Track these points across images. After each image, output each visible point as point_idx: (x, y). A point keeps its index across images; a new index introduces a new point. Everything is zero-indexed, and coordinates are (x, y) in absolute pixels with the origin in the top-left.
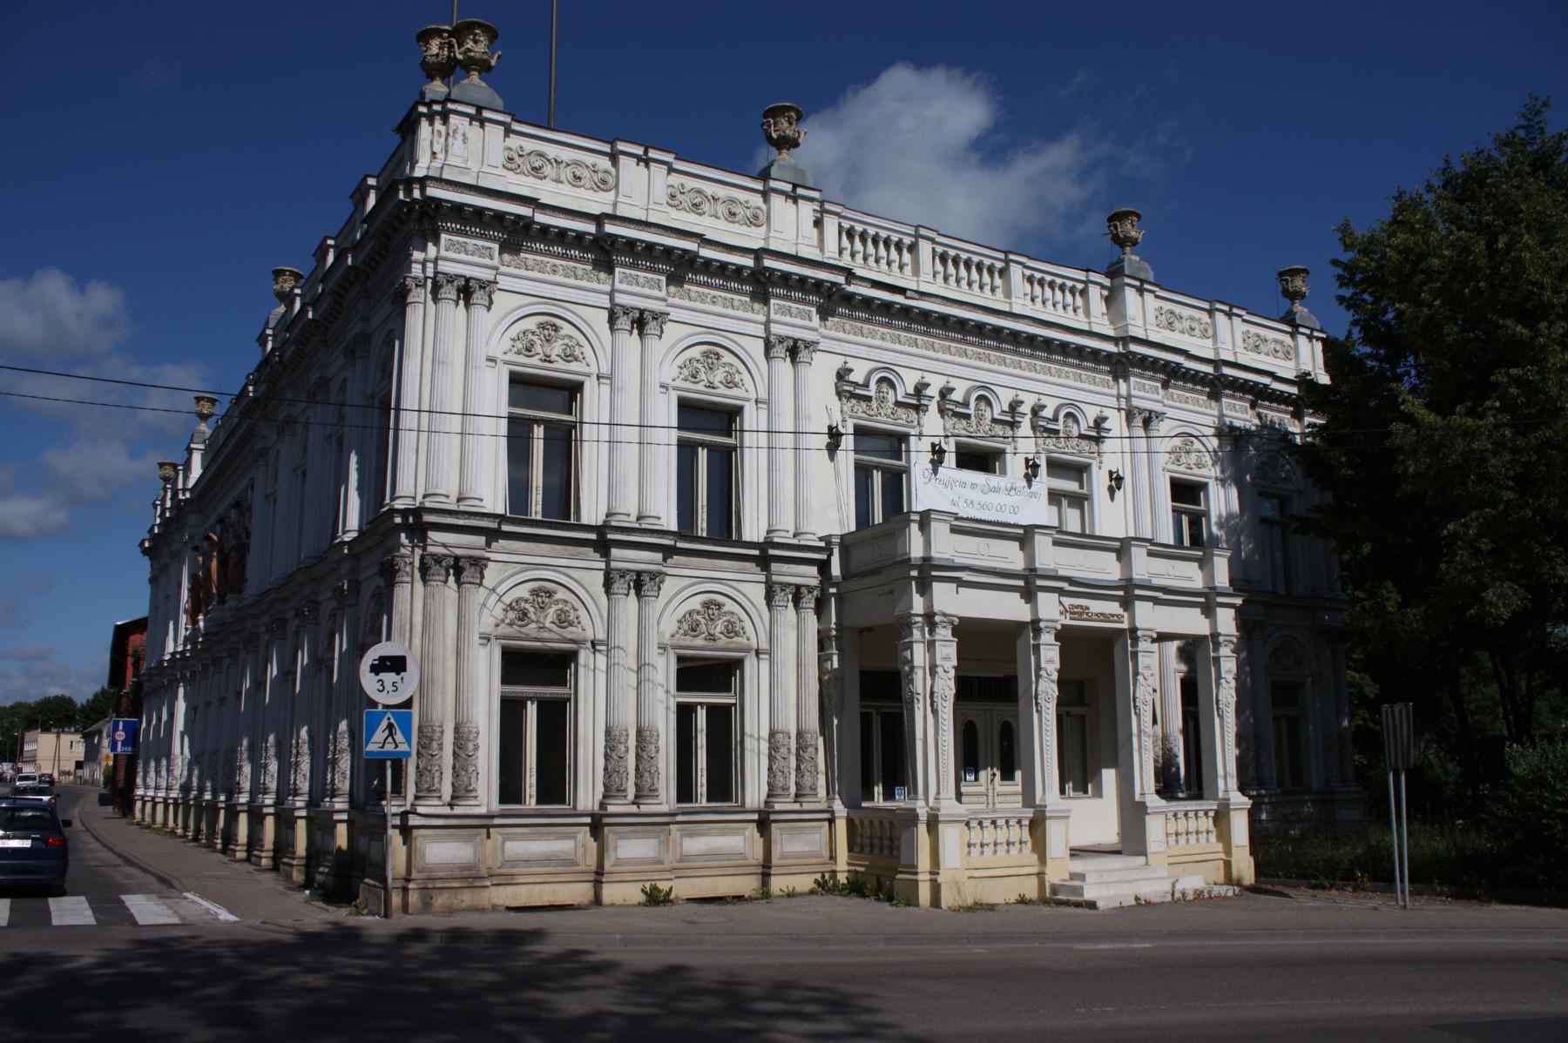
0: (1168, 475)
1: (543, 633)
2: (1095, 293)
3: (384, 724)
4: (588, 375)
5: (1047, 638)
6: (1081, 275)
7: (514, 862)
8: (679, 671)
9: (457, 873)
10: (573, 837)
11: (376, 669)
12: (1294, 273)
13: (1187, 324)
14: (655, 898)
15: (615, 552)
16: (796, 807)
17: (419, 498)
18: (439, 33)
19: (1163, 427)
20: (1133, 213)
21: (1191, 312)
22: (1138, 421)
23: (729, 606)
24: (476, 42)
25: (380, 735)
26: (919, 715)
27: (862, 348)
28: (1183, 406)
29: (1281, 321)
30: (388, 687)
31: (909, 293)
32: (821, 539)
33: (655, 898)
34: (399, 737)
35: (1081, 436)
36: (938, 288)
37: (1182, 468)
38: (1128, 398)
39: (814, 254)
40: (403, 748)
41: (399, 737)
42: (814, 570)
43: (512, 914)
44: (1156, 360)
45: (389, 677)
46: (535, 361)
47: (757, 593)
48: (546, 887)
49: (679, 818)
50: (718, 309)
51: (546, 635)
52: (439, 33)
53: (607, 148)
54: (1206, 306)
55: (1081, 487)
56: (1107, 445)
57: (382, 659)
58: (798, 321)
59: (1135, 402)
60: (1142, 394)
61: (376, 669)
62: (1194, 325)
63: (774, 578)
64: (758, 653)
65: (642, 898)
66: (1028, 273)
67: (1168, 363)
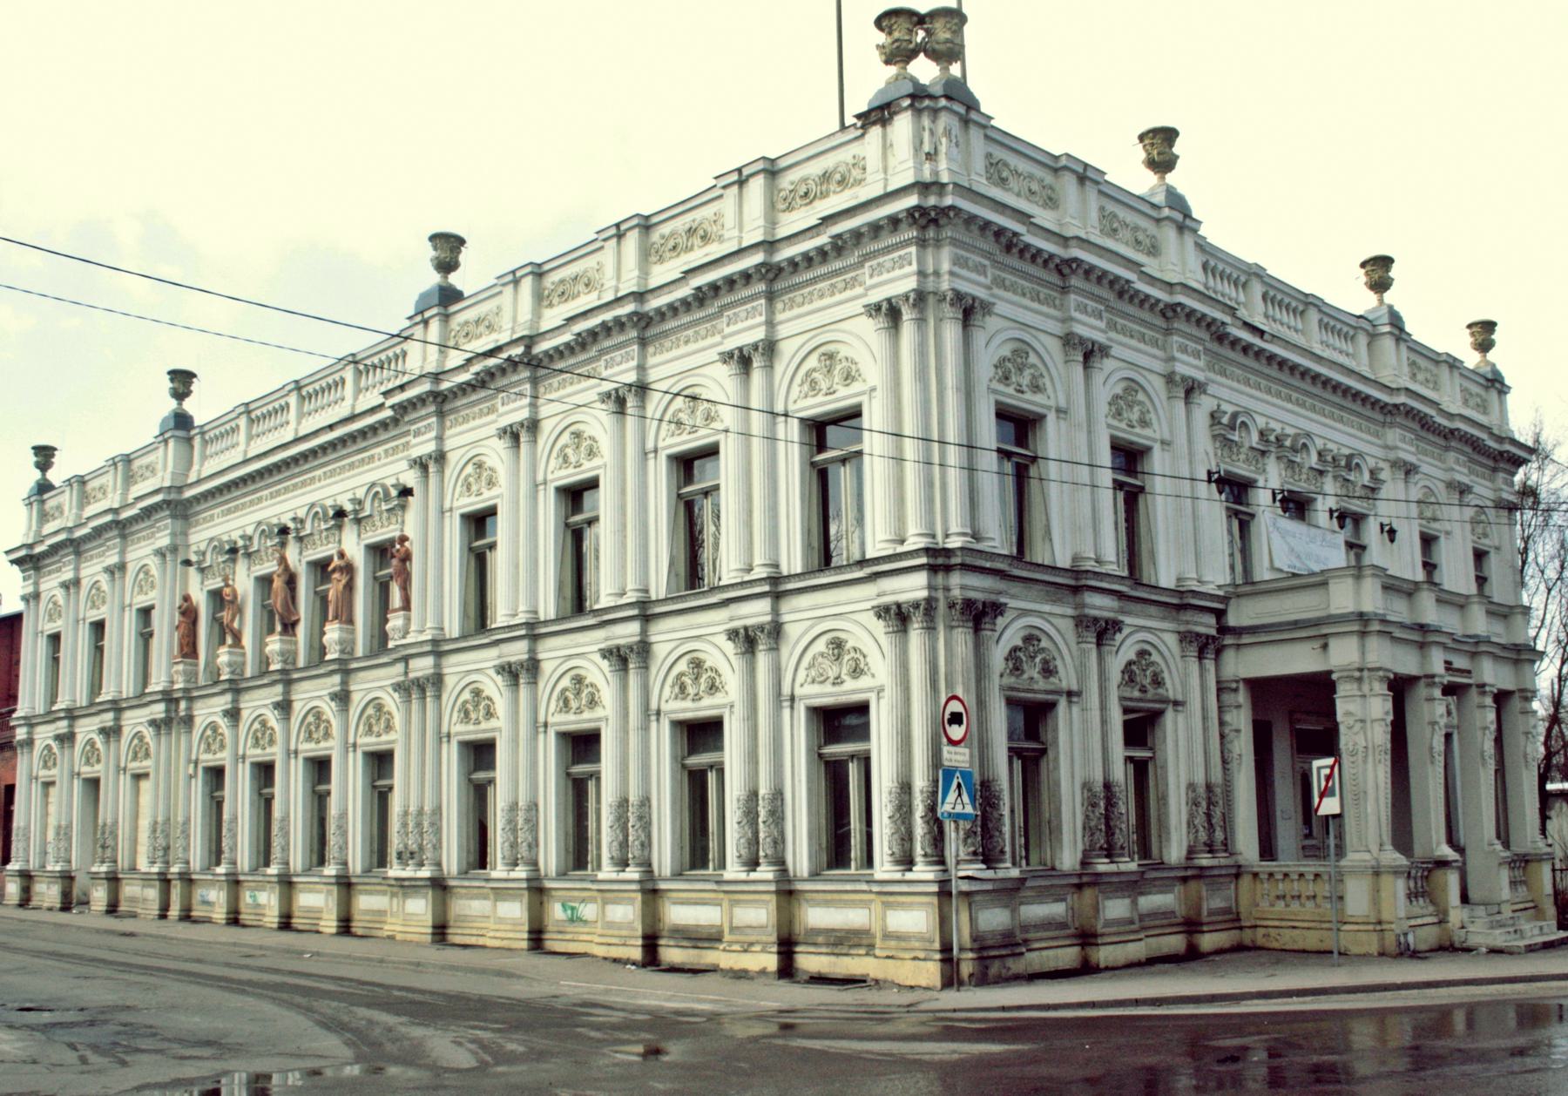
0: (992, 398)
4: (1049, 408)
7: (1025, 928)
8: (1126, 724)
23: (1155, 657)
27: (1229, 392)
31: (1266, 337)
36: (1318, 349)
37: (1123, 425)
39: (1365, 370)
42: (1212, 620)
44: (1105, 273)
46: (1010, 390)
48: (1051, 953)
66: (1326, 320)
67: (1117, 278)
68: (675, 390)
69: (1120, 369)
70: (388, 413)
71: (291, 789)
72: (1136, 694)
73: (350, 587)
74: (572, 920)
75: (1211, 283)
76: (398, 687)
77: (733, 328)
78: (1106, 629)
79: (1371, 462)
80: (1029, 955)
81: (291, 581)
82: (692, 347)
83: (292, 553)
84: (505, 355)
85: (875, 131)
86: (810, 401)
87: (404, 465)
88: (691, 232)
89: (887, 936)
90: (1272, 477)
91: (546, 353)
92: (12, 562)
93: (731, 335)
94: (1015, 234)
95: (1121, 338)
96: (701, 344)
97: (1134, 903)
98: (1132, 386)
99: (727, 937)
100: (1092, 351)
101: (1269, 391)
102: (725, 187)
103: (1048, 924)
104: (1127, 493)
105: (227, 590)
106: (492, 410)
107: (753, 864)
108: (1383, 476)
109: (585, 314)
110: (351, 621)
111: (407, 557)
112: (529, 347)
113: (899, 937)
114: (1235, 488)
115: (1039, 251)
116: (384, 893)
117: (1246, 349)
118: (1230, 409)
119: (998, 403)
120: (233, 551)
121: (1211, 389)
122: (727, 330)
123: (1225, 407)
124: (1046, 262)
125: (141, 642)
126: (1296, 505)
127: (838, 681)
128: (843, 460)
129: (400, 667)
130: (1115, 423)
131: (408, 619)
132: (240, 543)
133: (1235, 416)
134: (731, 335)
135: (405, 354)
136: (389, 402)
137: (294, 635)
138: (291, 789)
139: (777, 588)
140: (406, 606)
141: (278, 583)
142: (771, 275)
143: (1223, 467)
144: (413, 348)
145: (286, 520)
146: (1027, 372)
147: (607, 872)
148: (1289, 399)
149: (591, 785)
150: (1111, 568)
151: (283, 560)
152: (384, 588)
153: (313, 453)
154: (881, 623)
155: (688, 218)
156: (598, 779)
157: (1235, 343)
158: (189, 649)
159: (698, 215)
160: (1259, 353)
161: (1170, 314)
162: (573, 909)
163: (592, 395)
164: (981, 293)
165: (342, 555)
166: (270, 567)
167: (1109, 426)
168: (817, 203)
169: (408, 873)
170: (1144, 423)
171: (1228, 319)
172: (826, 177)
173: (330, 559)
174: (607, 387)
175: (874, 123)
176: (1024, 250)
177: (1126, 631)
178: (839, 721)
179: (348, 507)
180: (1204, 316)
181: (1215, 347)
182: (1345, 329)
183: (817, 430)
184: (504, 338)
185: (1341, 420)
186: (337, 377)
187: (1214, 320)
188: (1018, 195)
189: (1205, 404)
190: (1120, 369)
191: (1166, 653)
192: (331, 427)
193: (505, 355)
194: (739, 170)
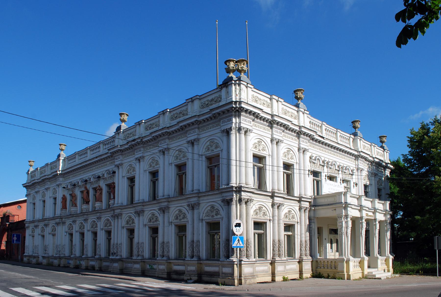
1: (260, 218)
2: (351, 140)
3: (237, 239)
5: (364, 221)
6: (349, 135)
9: (250, 275)
10: (266, 266)
11: (236, 226)
12: (298, 90)
13: (290, 114)
14: (285, 280)
15: (275, 198)
16: (280, 259)
17: (238, 184)
18: (233, 61)
19: (282, 145)
20: (302, 90)
21: (263, 97)
22: (359, 171)
24: (244, 65)
25: (236, 242)
26: (343, 237)
28: (288, 139)
29: (295, 106)
30: (238, 231)
32: (310, 196)
33: (285, 280)
34: (241, 242)
35: (350, 174)
38: (358, 165)
40: (242, 245)
41: (241, 242)
42: (308, 203)
43: (259, 284)
45: (238, 228)
47: (297, 208)
49: (258, 262)
50: (290, 140)
51: (261, 218)
52: (233, 61)
53: (269, 96)
54: (370, 144)
55: (347, 185)
56: (354, 176)
57: (237, 224)
58: (248, 123)
59: (359, 166)
60: (277, 134)
61: (236, 226)
62: (265, 103)
63: (302, 205)
64: (270, 220)
65: (282, 279)
66: (342, 135)
68: (177, 149)
69: (255, 136)
70: (109, 154)
71: (88, 238)
72: (288, 220)
73: (101, 193)
74: (151, 268)
75: (312, 126)
76: (112, 216)
77: (189, 136)
78: (248, 201)
79: (352, 168)
80: (257, 278)
81: (88, 192)
82: (180, 140)
83: (88, 186)
84: (136, 141)
85: (224, 90)
86: (208, 153)
87: (114, 166)
88: (180, 113)
89: (223, 273)
90: (325, 172)
91: (146, 141)
92: (24, 187)
93: (189, 137)
94: (259, 114)
95: (286, 139)
96: (182, 139)
97: (285, 267)
98: (289, 150)
99: (186, 273)
100: (247, 131)
101: (326, 151)
102: (188, 102)
103: (263, 271)
104: (287, 175)
105: (73, 194)
106: (134, 154)
107: (192, 257)
108: (354, 171)
109: (155, 132)
110: (101, 201)
111: (114, 187)
112: (142, 139)
113: (225, 274)
114: (315, 174)
115: (265, 118)
116: (109, 262)
117: (319, 142)
118: (315, 155)
119: (253, 154)
120: (74, 185)
121: (310, 151)
122: (188, 136)
123: (313, 155)
124: (281, 125)
125: (54, 205)
126: (331, 178)
127: (213, 216)
128: (215, 166)
129: (112, 212)
130: (284, 158)
131: (114, 201)
132: (76, 183)
133: (316, 157)
134: (189, 137)
135: (114, 141)
136: (109, 152)
137: (89, 204)
138: (88, 238)
139: (199, 194)
140: (114, 198)
141: (85, 192)
142: (198, 123)
143: (329, 174)
144: (117, 140)
145: (87, 178)
146: (290, 155)
147: (159, 258)
148: (331, 153)
149: (156, 239)
150: (282, 192)
151: (86, 188)
152: (110, 194)
153: (93, 163)
154: (223, 203)
155: (180, 109)
156: (186, 236)
157: (316, 141)
158: (64, 207)
159: (182, 109)
160: (323, 143)
161: (299, 133)
162: (151, 266)
163: (157, 151)
164: (307, 148)
165: (99, 186)
166: (83, 189)
167: (283, 159)
168: (210, 106)
169: (114, 257)
170: (292, 158)
171: (314, 134)
172: (212, 100)
173: (97, 187)
174: (160, 149)
175: (224, 87)
176: (261, 118)
177: (285, 206)
178: (289, 227)
179: (101, 176)
180: (308, 134)
181: (311, 141)
182: (347, 137)
183: (209, 159)
184: (136, 137)
185: (344, 158)
186: (98, 146)
187: (311, 135)
188: (261, 104)
189: (308, 155)
190: (255, 136)
191: (296, 211)
192: (96, 157)
193: (136, 141)
194: (191, 98)
